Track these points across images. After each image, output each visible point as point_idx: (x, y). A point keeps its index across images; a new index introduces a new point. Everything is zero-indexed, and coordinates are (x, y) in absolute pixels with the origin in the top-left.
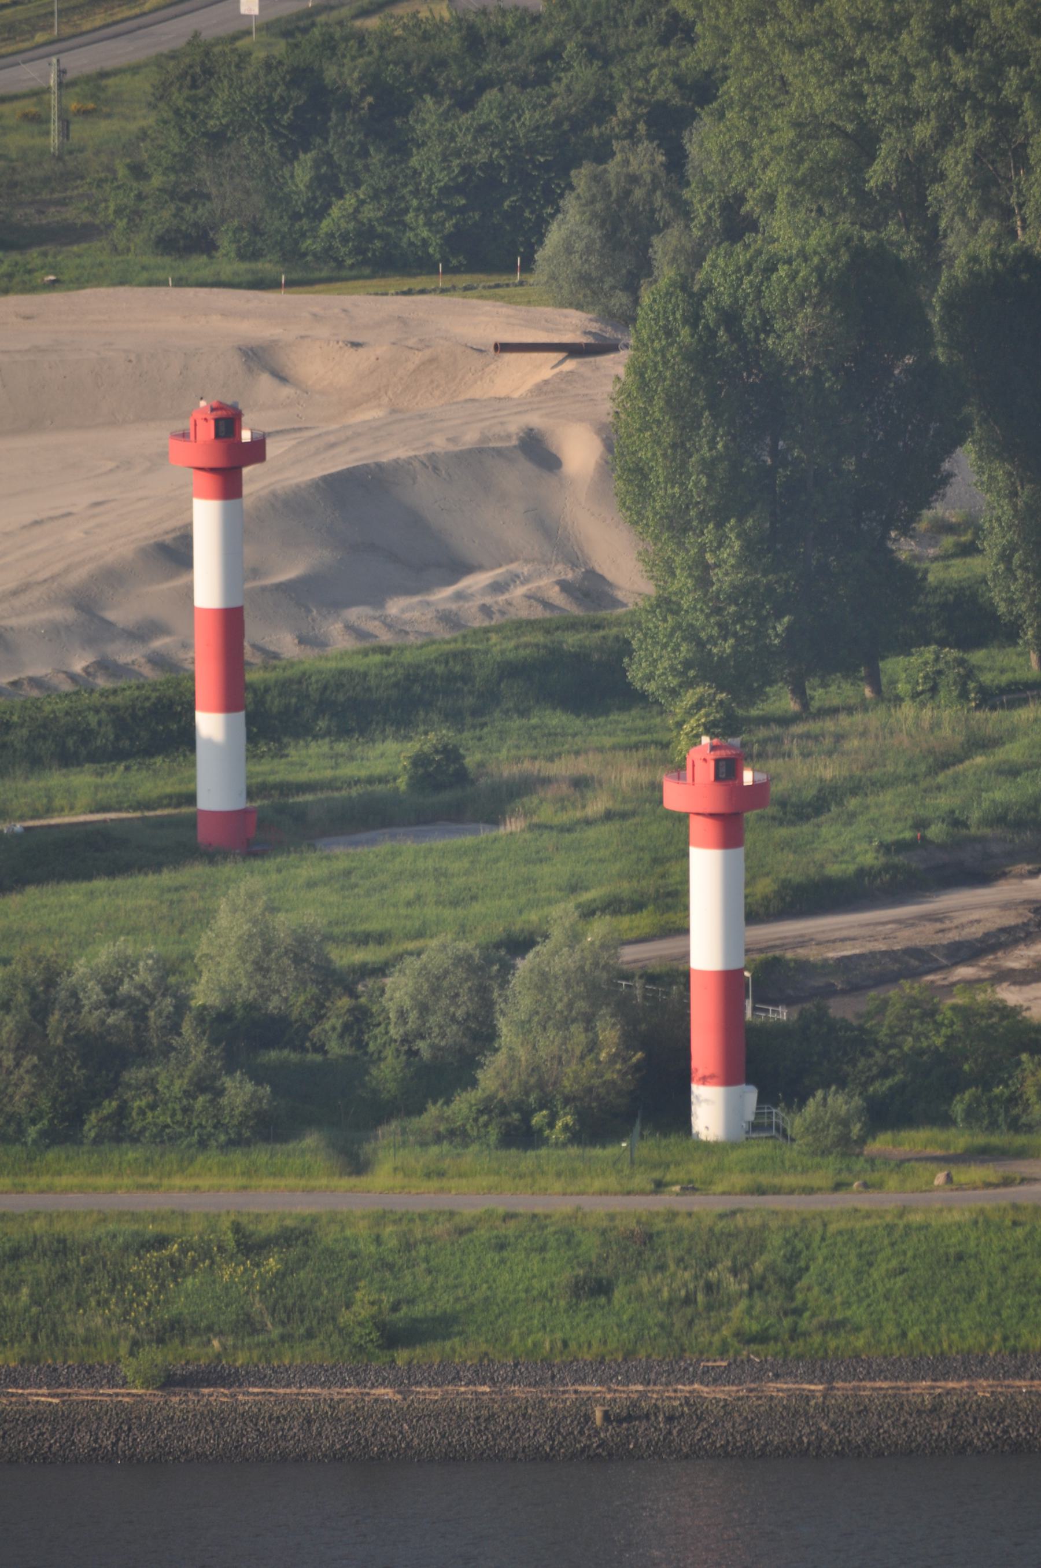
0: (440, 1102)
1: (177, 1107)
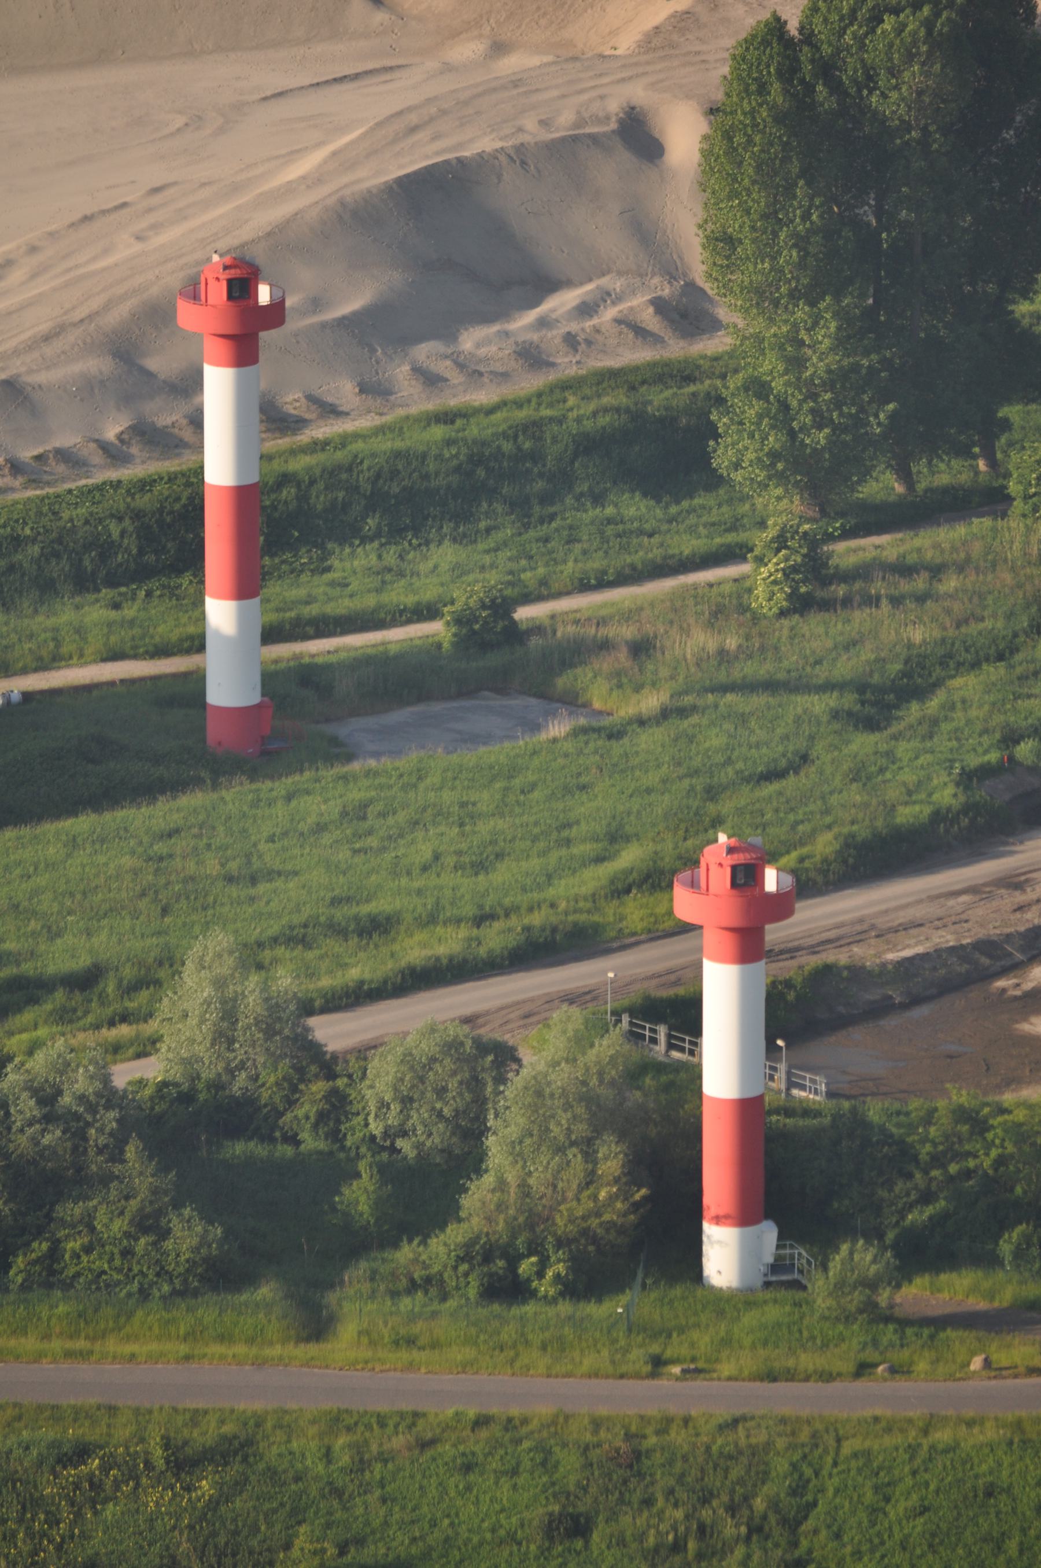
0: (416, 1242)
1: (116, 1251)
